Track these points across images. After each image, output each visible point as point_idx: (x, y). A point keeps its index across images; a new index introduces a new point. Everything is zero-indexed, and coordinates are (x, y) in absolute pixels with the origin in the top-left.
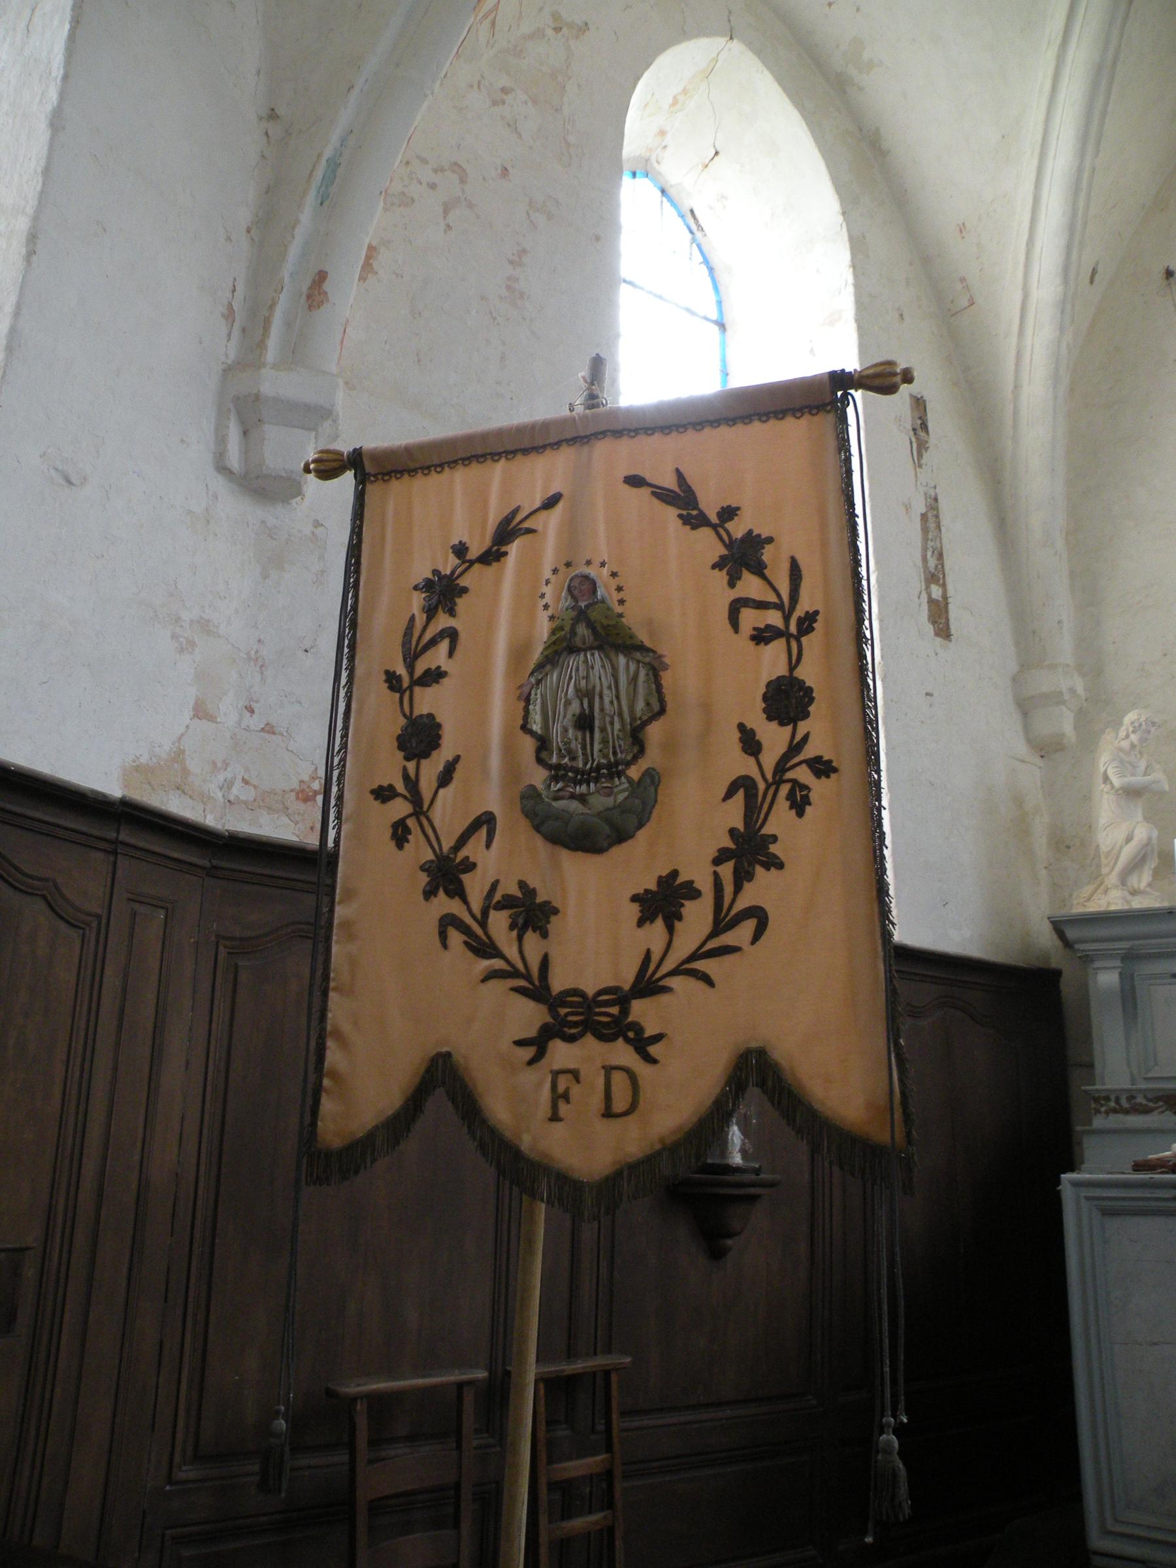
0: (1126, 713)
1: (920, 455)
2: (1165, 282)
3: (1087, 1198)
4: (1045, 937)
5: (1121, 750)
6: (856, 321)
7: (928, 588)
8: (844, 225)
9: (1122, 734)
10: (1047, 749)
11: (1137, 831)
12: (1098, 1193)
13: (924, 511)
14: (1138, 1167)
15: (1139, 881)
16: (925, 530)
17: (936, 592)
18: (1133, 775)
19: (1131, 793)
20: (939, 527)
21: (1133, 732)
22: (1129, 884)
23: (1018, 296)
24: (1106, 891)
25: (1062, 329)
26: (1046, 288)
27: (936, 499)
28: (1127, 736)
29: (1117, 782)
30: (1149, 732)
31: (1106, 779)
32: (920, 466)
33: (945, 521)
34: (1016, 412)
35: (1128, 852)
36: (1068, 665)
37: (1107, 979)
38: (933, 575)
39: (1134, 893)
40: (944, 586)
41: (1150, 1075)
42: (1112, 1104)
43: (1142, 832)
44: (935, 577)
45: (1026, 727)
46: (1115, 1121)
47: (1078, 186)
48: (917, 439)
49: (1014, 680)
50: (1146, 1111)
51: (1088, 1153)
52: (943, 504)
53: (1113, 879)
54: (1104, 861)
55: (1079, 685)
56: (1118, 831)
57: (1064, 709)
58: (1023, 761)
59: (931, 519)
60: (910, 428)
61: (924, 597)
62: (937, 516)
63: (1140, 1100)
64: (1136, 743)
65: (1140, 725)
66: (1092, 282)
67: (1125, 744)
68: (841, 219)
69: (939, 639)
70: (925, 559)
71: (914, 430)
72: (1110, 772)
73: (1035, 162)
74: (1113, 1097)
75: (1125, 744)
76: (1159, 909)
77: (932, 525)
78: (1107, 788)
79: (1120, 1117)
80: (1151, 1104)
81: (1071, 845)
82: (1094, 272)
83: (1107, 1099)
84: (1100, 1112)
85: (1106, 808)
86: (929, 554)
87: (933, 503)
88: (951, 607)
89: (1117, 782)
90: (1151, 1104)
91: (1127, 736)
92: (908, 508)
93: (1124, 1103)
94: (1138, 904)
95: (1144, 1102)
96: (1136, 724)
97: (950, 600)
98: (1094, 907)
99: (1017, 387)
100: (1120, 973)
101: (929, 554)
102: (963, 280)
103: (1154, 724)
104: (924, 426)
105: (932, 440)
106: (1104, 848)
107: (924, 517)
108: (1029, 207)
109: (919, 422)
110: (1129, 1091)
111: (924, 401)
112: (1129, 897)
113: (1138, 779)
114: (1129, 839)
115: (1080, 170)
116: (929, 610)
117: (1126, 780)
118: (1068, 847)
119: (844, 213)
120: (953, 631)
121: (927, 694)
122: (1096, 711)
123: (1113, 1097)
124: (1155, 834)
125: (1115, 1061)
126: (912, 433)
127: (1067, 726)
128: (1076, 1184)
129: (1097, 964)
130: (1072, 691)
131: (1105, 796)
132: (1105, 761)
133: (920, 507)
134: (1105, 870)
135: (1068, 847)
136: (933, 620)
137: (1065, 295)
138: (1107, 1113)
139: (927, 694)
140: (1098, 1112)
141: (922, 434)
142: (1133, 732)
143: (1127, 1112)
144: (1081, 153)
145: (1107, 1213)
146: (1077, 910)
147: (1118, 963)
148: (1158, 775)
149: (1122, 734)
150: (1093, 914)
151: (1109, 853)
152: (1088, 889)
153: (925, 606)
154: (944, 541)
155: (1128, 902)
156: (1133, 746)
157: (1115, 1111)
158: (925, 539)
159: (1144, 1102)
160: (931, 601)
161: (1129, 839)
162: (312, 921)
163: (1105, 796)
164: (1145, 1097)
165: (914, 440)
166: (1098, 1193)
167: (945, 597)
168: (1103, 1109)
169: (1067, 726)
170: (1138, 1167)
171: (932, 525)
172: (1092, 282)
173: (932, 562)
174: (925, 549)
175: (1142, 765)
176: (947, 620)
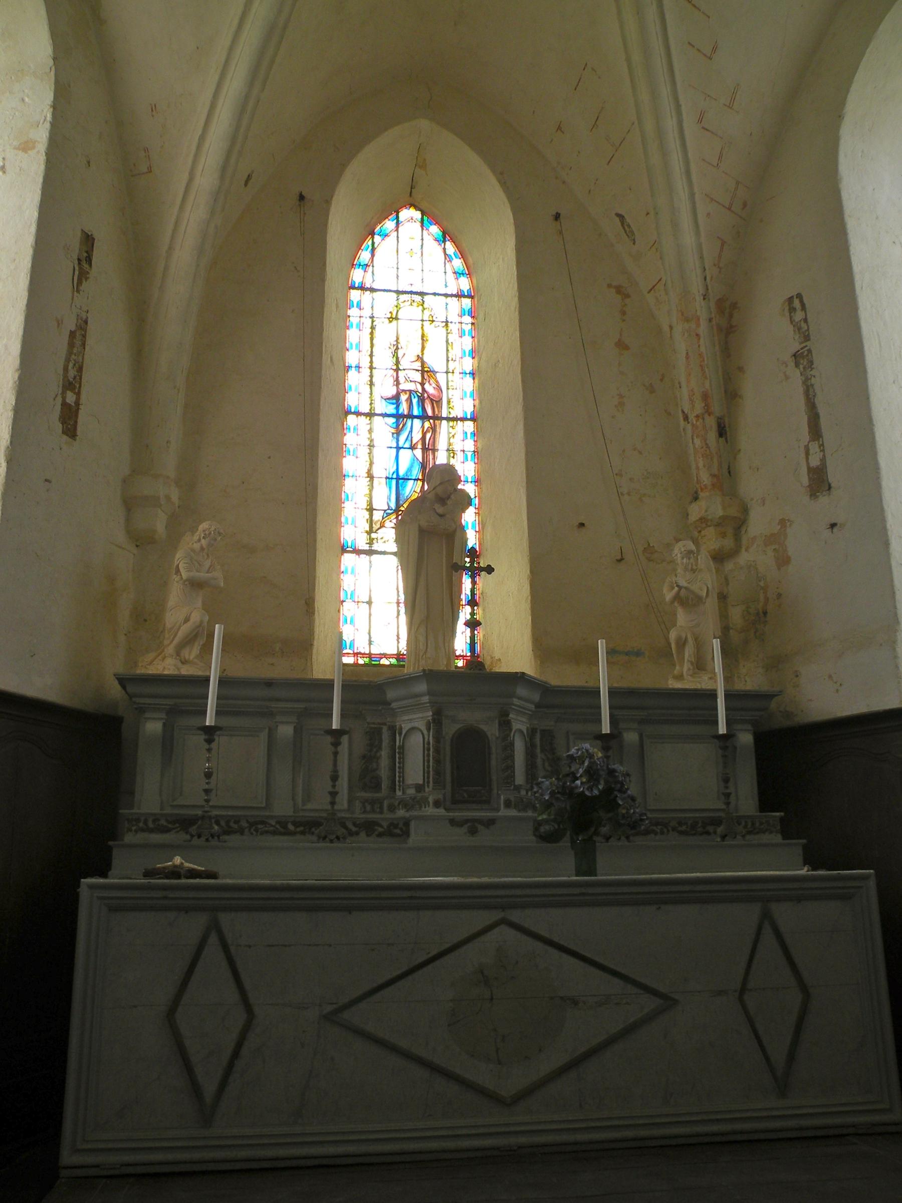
0: (201, 522)
1: (80, 282)
2: (298, 203)
3: (99, 898)
4: (115, 691)
5: (193, 550)
6: (46, 154)
7: (64, 393)
8: (53, 69)
9: (196, 538)
10: (141, 540)
11: (193, 615)
12: (106, 894)
13: (73, 328)
14: (148, 874)
15: (190, 652)
16: (71, 345)
17: (71, 398)
18: (197, 571)
19: (195, 585)
20: (84, 345)
21: (204, 538)
22: (182, 655)
23: (185, 176)
24: (164, 659)
25: (213, 213)
26: (206, 179)
27: (86, 322)
28: (199, 540)
29: (185, 575)
30: (216, 540)
31: (178, 571)
32: (78, 291)
33: (90, 341)
34: (166, 268)
35: (185, 629)
36: (168, 477)
37: (153, 727)
38: (70, 383)
39: (184, 662)
40: (78, 394)
41: (175, 803)
42: (141, 825)
43: (196, 617)
44: (72, 385)
45: (128, 520)
46: (141, 838)
47: (245, 108)
48: (80, 268)
49: (124, 481)
50: (166, 830)
51: (116, 862)
52: (92, 326)
53: (170, 650)
54: (167, 636)
55: (175, 496)
56: (181, 612)
57: (160, 511)
58: (120, 547)
59: (78, 336)
60: (76, 257)
61: (59, 400)
62: (84, 336)
63: (163, 822)
64: (204, 546)
65: (210, 533)
66: (246, 184)
67: (197, 546)
68: (51, 62)
69: (65, 437)
70: (66, 369)
71: (79, 260)
72: (182, 567)
73: (217, 77)
74: (143, 819)
75: (197, 546)
76: (198, 677)
77: (78, 342)
78: (177, 578)
79: (145, 835)
80: (170, 826)
81: (147, 618)
82: (249, 177)
83: (138, 820)
84: (131, 831)
85: (175, 593)
86: (71, 365)
87: (83, 325)
88: (80, 412)
89: (185, 575)
90: (170, 826)
91: (199, 540)
92: (59, 323)
93: (151, 825)
94: (186, 671)
95: (165, 824)
96: (207, 532)
97: (81, 407)
98: (152, 670)
99: (171, 248)
100: (164, 724)
101: (71, 365)
102: (146, 150)
103: (220, 534)
104: (89, 260)
105: (94, 272)
106: (168, 625)
107: (72, 334)
108: (206, 111)
109: (85, 255)
110: (155, 814)
111: (94, 239)
112: (180, 664)
113: (203, 575)
114: (187, 620)
115: (247, 97)
116: (61, 412)
117: (192, 574)
118: (145, 620)
119: (55, 59)
120: (78, 433)
121: (46, 480)
122: (183, 518)
123: (143, 819)
124: (207, 618)
125: (150, 792)
126: (76, 262)
127: (160, 527)
128: (92, 887)
129: (147, 715)
130: (168, 498)
131: (176, 584)
132: (180, 558)
133: (71, 324)
134: (166, 642)
135: (145, 620)
136: (64, 420)
137: (220, 187)
138: (136, 831)
139: (46, 480)
140: (130, 830)
141: (85, 266)
142: (204, 538)
143: (151, 831)
144: (251, 84)
145: (113, 909)
146: (140, 671)
147: (163, 716)
148: (218, 574)
149: (196, 538)
150: (153, 675)
151: (171, 629)
152: (151, 655)
153: (58, 407)
154: (86, 357)
155: (179, 669)
156: (202, 549)
157: (143, 830)
158: (70, 353)
159: (165, 824)
160: (64, 404)
161: (187, 620)
162: (401, 481)
163: (176, 584)
164: (167, 821)
165: (77, 268)
166: (106, 894)
167: (77, 403)
168: (134, 828)
169: (160, 527)
170: (148, 874)
171: (78, 342)
172: (246, 184)
173: (72, 373)
174: (68, 360)
175: (207, 564)
176: (76, 422)
